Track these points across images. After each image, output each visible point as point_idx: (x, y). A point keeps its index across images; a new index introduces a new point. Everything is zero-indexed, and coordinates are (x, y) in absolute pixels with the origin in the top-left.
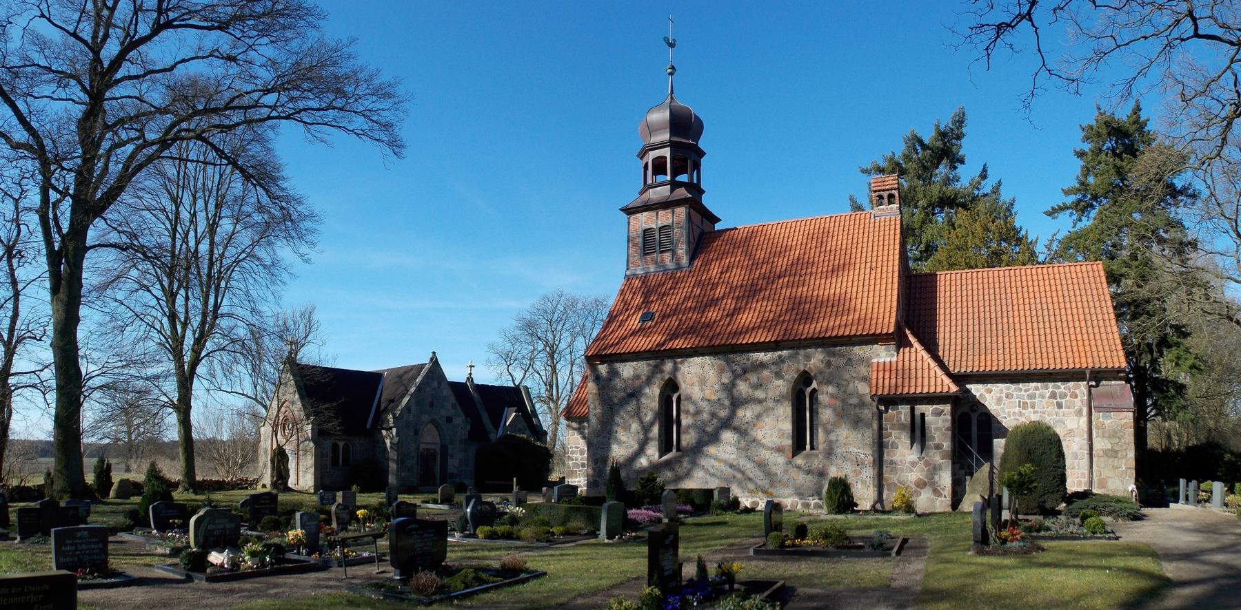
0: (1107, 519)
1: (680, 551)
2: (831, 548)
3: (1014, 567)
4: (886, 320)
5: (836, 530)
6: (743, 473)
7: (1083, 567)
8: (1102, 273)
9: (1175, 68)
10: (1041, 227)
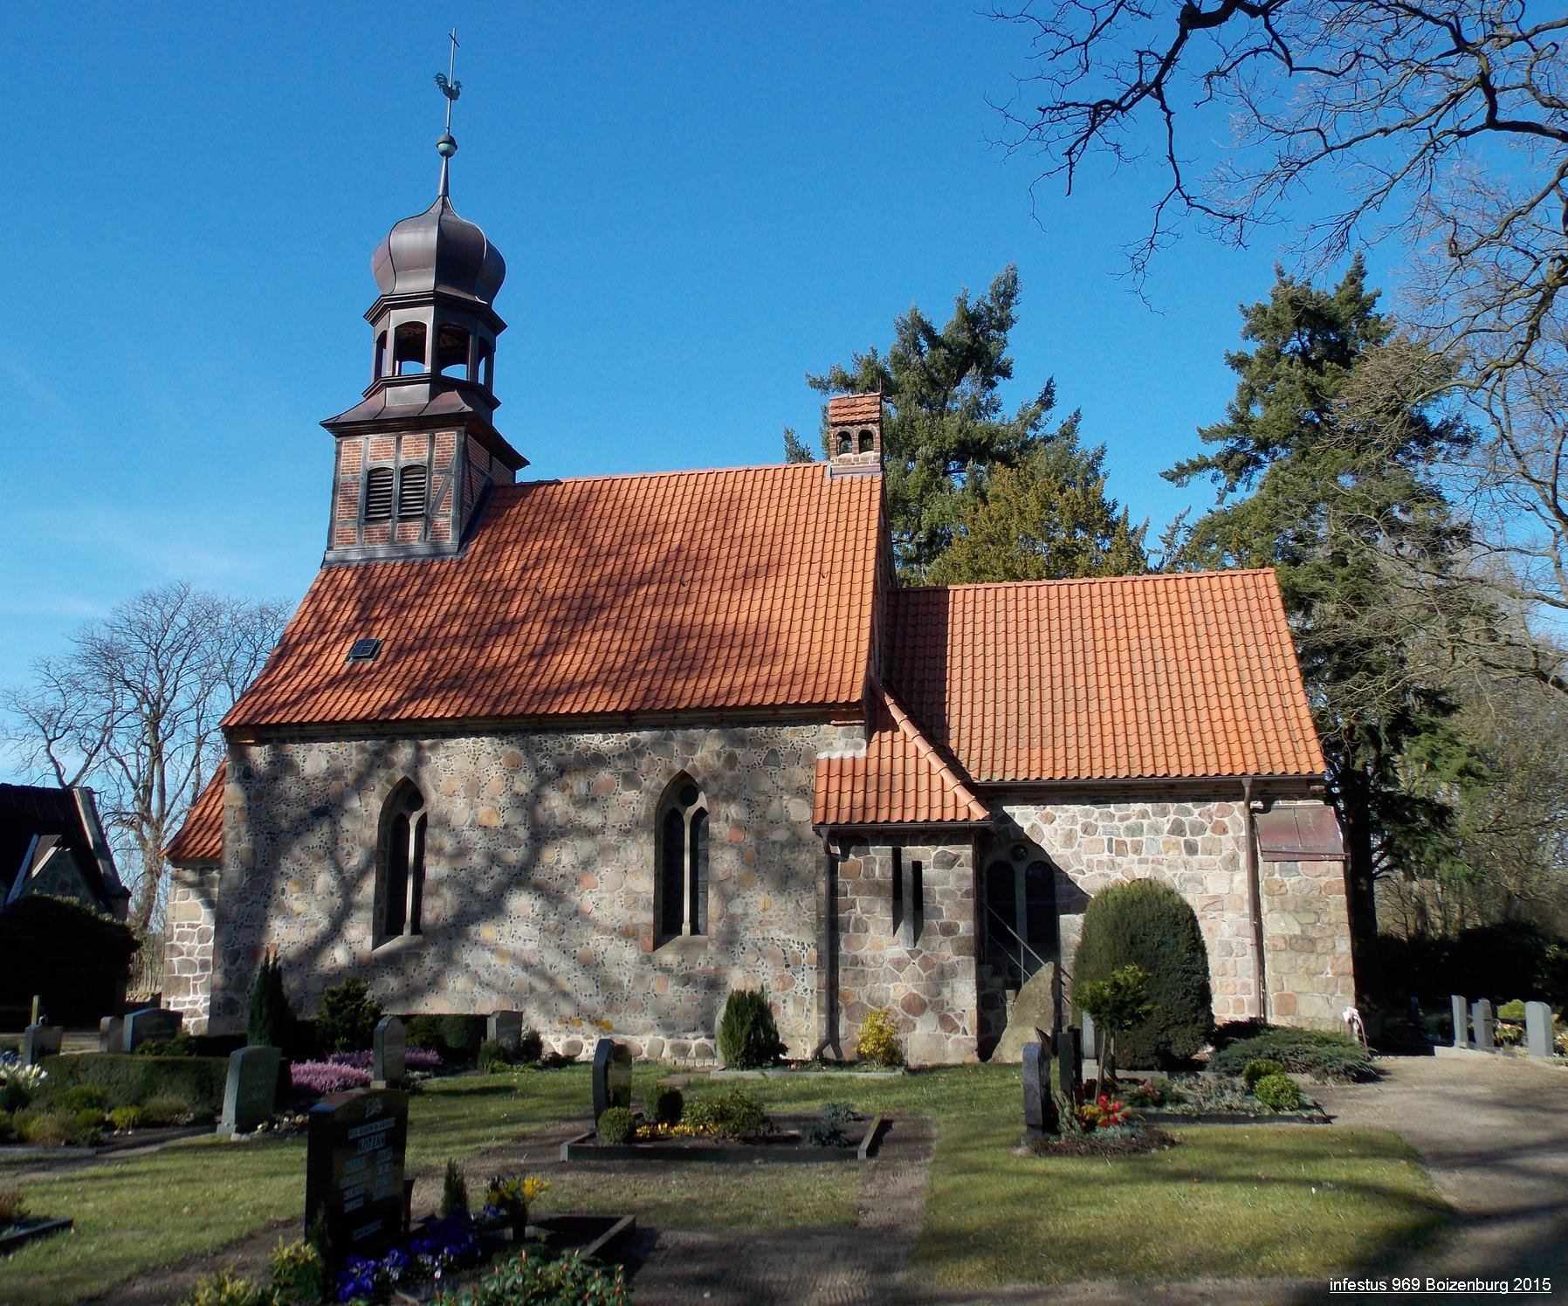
0: (1303, 1080)
1: (410, 1153)
2: (732, 1143)
3: (1112, 1182)
4: (847, 677)
5: (742, 1102)
6: (551, 981)
7: (1259, 1181)
8: (1275, 591)
9: (1441, 191)
10: (1154, 506)
